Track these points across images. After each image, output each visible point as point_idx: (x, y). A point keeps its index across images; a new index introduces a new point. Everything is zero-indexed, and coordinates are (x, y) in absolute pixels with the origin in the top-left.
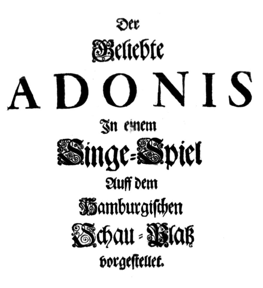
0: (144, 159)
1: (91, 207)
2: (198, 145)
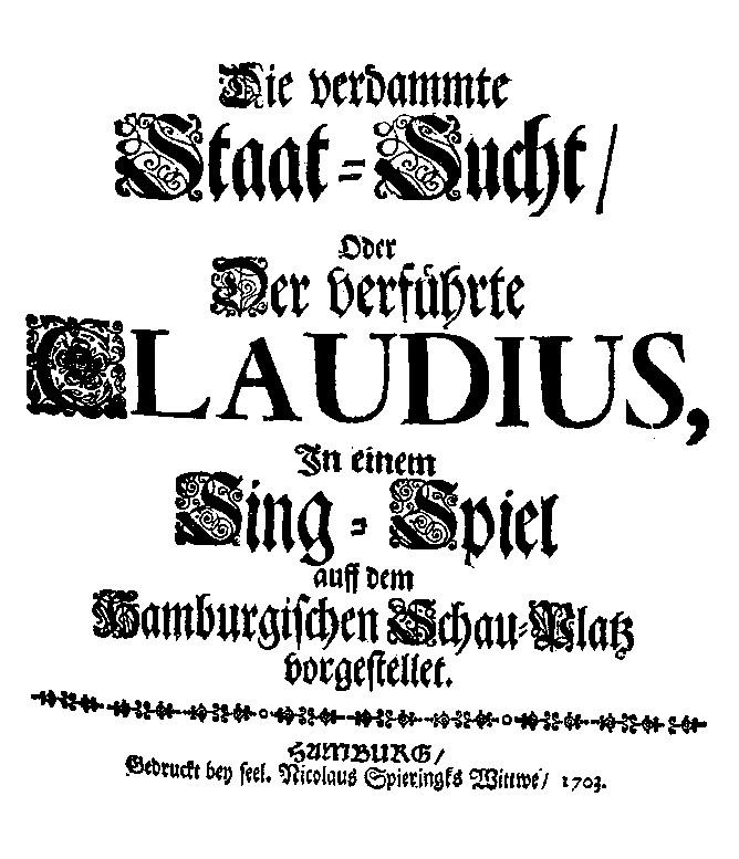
0: (405, 535)
1: (123, 614)
2: (548, 504)
